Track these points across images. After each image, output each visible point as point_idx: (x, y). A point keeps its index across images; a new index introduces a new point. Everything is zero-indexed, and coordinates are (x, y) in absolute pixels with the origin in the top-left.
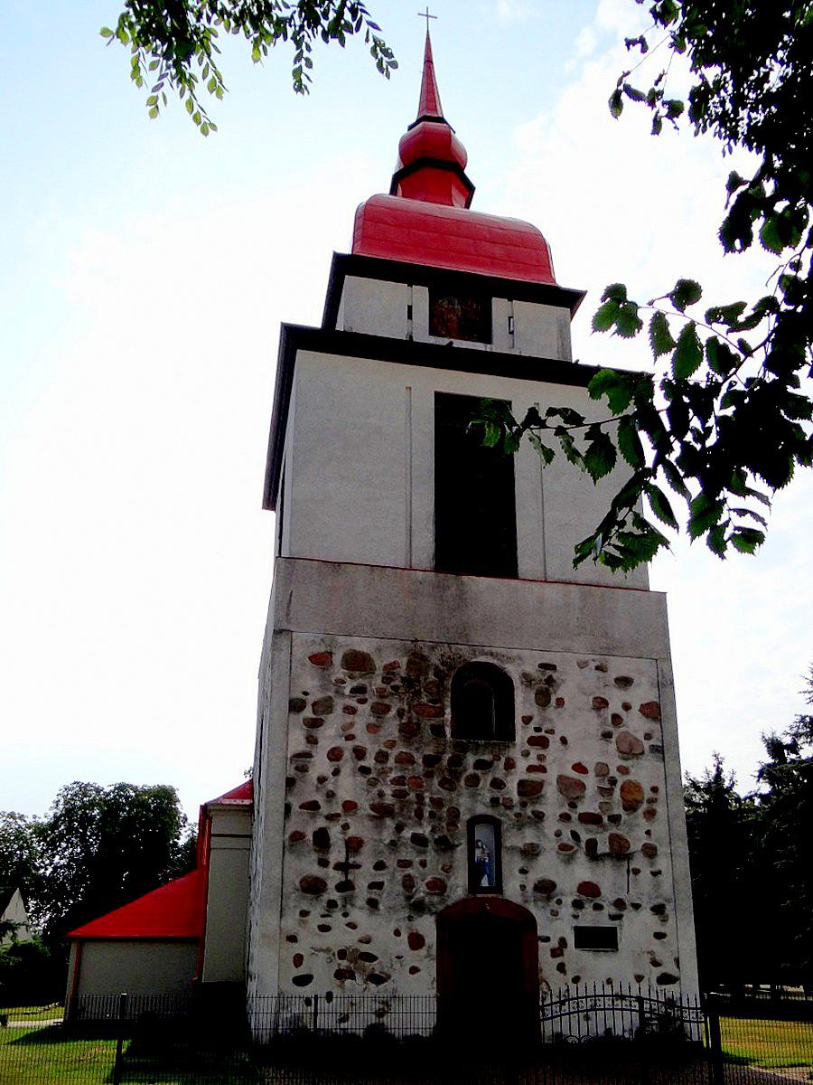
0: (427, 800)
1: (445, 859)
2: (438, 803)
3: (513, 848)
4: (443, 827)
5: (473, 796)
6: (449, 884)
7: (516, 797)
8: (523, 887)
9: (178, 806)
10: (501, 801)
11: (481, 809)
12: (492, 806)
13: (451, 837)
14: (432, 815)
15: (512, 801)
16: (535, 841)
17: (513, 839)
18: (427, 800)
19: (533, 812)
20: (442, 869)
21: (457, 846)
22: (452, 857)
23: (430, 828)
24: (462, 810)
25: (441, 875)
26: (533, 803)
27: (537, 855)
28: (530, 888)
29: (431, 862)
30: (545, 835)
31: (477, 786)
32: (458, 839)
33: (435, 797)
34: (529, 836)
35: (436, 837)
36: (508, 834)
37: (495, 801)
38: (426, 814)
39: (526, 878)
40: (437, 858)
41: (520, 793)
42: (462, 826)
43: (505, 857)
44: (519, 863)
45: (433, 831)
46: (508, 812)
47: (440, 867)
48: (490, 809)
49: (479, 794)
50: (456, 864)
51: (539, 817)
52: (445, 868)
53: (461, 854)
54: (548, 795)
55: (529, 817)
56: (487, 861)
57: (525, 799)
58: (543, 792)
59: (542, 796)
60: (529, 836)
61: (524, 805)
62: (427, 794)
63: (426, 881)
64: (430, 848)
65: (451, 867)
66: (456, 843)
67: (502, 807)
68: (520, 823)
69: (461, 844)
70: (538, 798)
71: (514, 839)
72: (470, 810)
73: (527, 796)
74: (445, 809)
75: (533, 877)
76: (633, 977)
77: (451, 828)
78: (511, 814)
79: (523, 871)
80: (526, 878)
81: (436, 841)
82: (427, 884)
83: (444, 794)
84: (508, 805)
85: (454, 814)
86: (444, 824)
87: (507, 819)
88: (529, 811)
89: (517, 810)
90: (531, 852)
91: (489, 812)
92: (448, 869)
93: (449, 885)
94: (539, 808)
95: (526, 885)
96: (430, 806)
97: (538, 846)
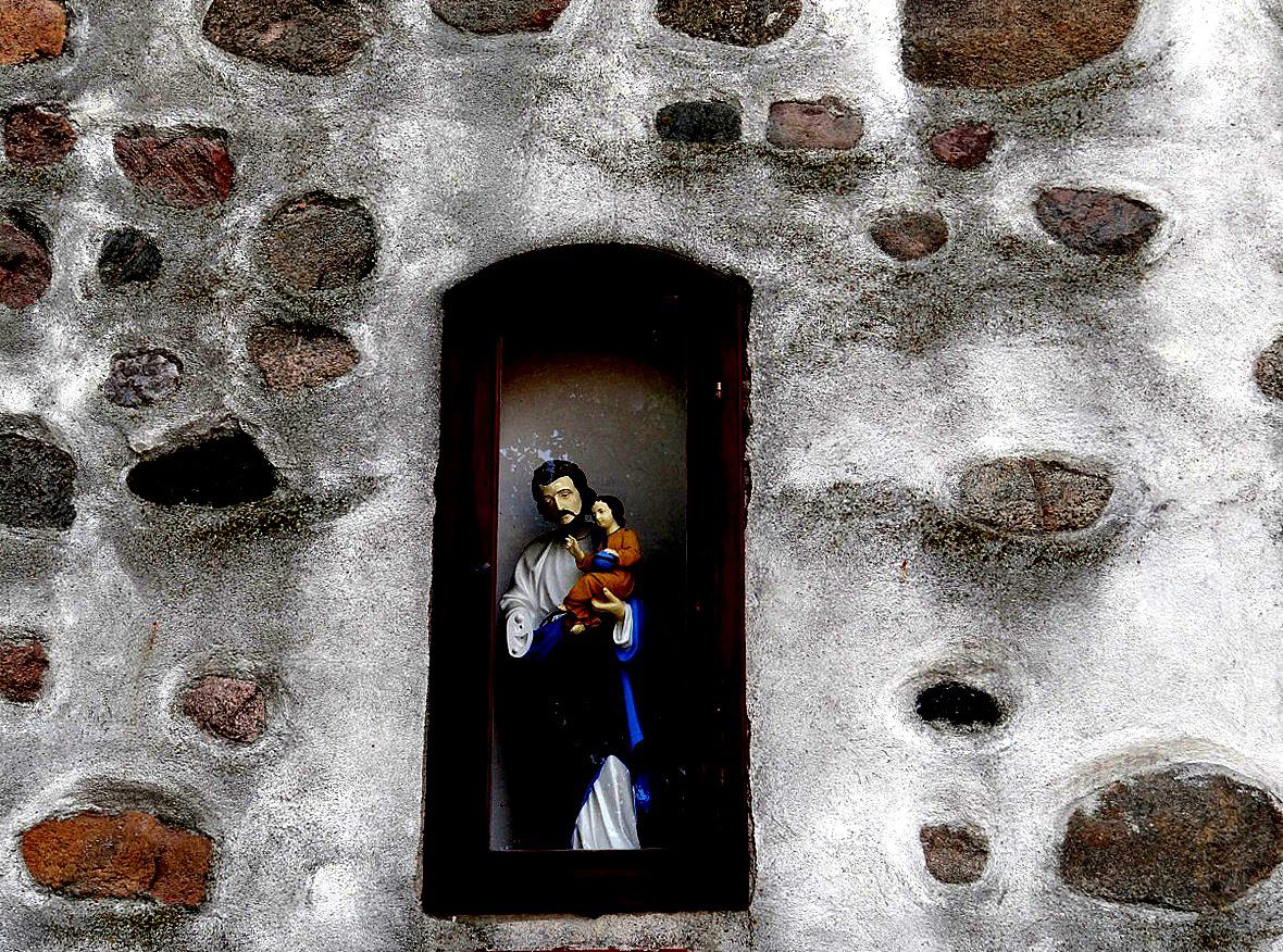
0: (95, 153)
1: (218, 621)
2: (202, 169)
3: (855, 509)
4: (215, 359)
5: (504, 103)
6: (238, 834)
7: (885, 96)
8: (954, 851)
9: (1090, 806)
10: (753, 128)
11: (564, 201)
12: (670, 172)
13: (285, 422)
14: (127, 261)
15: (846, 117)
16: (1067, 437)
17: (855, 423)
18: (95, 153)
19: (1046, 203)
20: (190, 707)
21: (340, 504)
22: (280, 598)
23: (97, 369)
24: (395, 212)
25: (168, 758)
26: (1059, 131)
27: (1093, 557)
28: (1023, 850)
29: (86, 643)
30: (1159, 388)
31: (544, 23)
32: (352, 446)
33: (167, 121)
34: (1014, 398)
35: (151, 435)
36: (816, 386)
37: (695, 131)
38: (75, 260)
39: (986, 768)
40: (139, 607)
41: (922, 64)
42: (390, 347)
43: (781, 590)
44: (908, 627)
45: (127, 388)
46: (813, 211)
47: (167, 688)
48: (648, 194)
49: (558, 83)
50: (315, 658)
51: (1110, 242)
52: (222, 691)
53: (364, 589)
54: (1183, 64)
55: (1009, 247)
56: (624, 635)
57: (969, 106)
58: (1140, 45)
59: (1132, 77)
60: (1014, 398)
61: (963, 152)
62: (96, 106)
63: (28, 814)
64: (87, 527)
65: (268, 684)
66: (329, 478)
67: (762, 172)
68: (927, 296)
69: (369, 487)
70: (1092, 90)
71: (844, 429)
72: (463, 210)
73: (995, 81)
74: (247, 213)
75: (1048, 764)
76: (915, 833)
77: (301, 359)
78: (843, 226)
79: (954, 705)
80: (986, 768)
81: (159, 479)
82: (32, 843)
83: (247, 96)
84: (821, 154)
85: (333, 245)
86: (228, 332)
87: (798, 269)
88: (1008, 197)
89: (901, 190)
90: (1030, 539)
91: (644, 216)
92: (235, 710)
93: (234, 846)
94: (1098, 166)
95: (986, 824)
96: (109, 193)
97: (1101, 481)
